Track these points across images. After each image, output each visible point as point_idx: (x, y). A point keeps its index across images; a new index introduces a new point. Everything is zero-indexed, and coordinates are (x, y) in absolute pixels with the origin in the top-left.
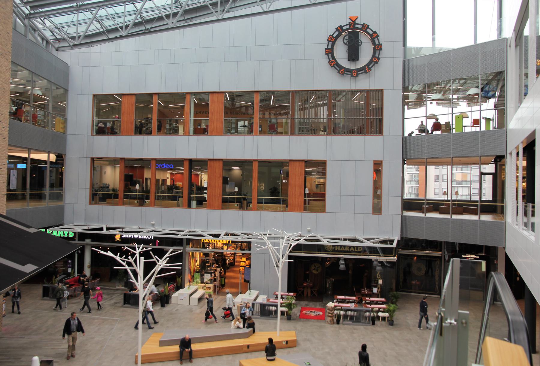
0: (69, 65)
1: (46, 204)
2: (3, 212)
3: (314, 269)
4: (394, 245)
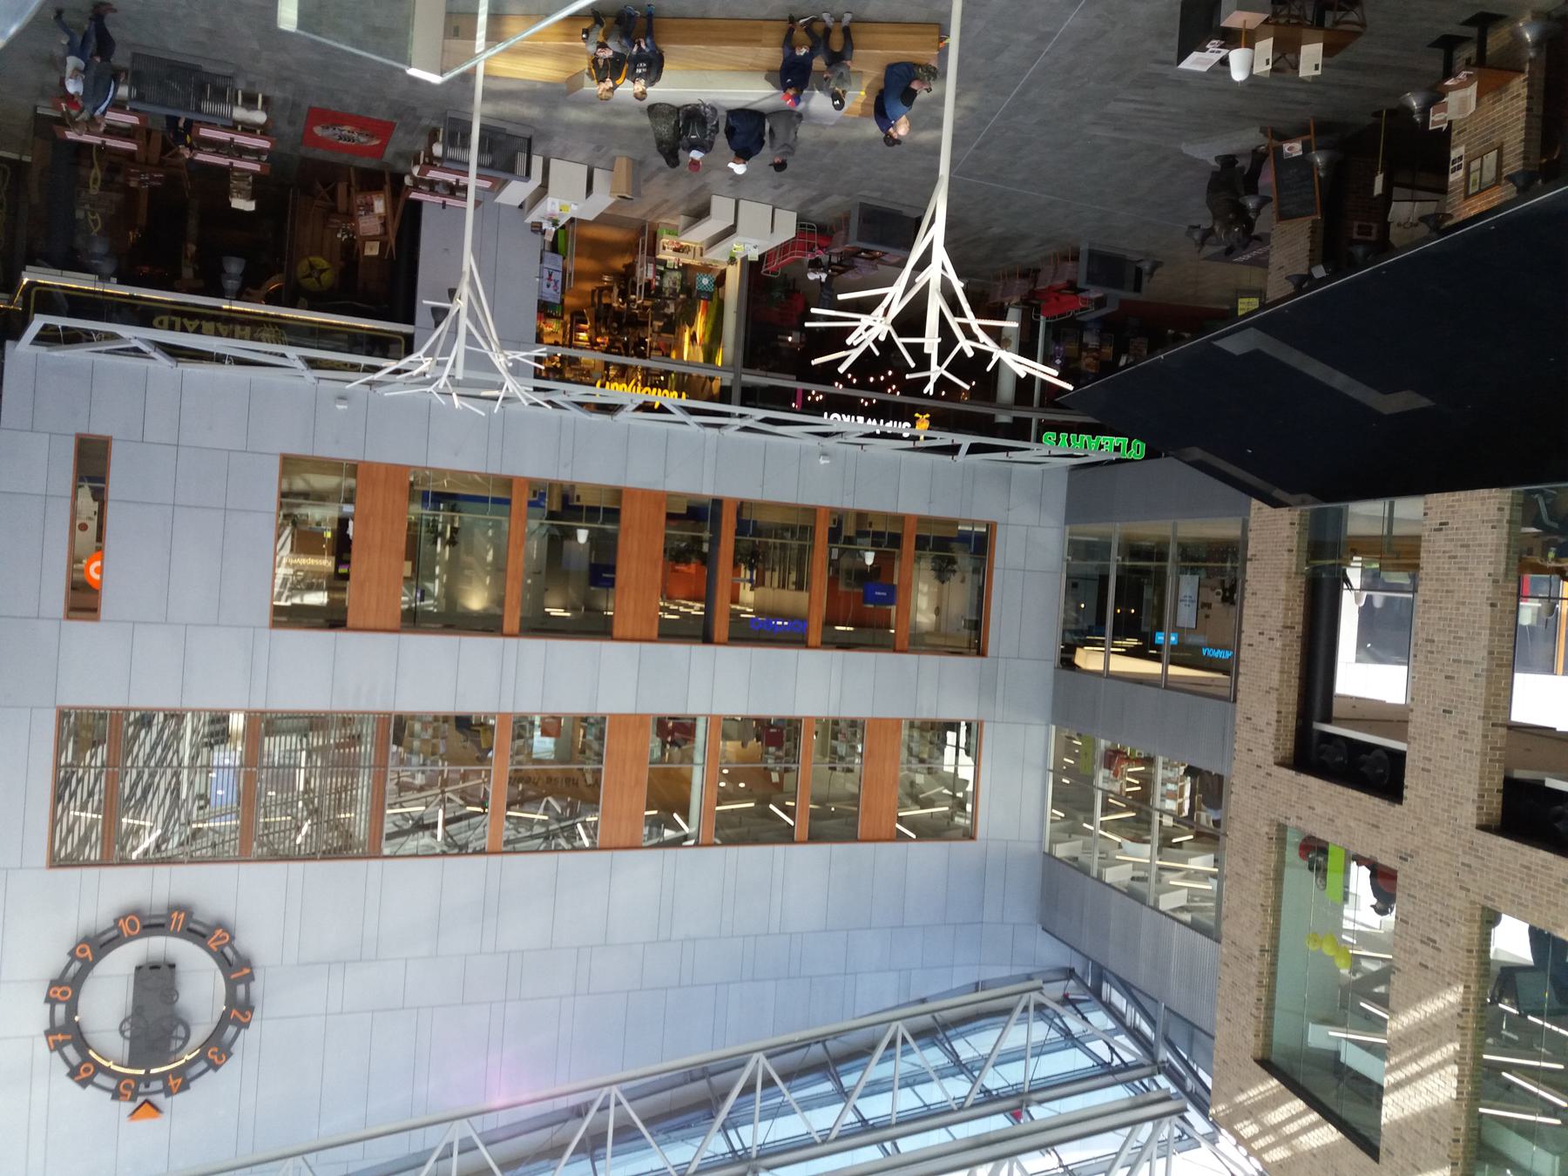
0: (1039, 928)
1: (1115, 530)
2: (1259, 509)
3: (323, 271)
4: (38, 322)
